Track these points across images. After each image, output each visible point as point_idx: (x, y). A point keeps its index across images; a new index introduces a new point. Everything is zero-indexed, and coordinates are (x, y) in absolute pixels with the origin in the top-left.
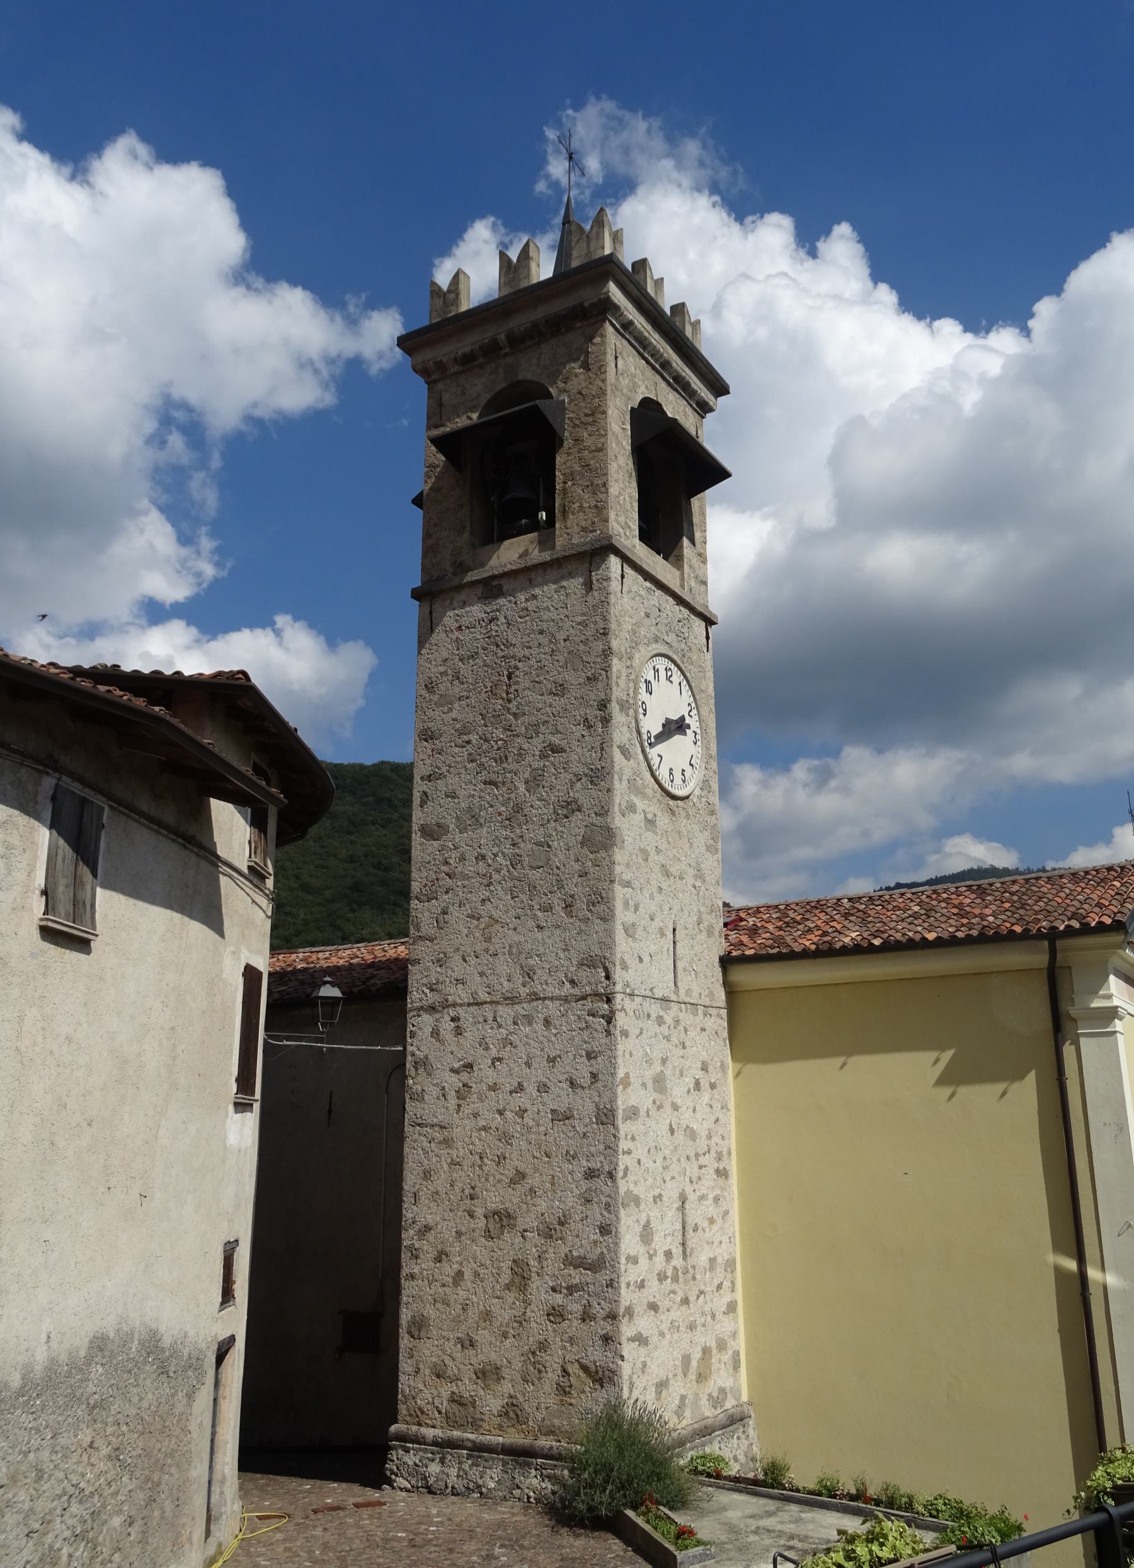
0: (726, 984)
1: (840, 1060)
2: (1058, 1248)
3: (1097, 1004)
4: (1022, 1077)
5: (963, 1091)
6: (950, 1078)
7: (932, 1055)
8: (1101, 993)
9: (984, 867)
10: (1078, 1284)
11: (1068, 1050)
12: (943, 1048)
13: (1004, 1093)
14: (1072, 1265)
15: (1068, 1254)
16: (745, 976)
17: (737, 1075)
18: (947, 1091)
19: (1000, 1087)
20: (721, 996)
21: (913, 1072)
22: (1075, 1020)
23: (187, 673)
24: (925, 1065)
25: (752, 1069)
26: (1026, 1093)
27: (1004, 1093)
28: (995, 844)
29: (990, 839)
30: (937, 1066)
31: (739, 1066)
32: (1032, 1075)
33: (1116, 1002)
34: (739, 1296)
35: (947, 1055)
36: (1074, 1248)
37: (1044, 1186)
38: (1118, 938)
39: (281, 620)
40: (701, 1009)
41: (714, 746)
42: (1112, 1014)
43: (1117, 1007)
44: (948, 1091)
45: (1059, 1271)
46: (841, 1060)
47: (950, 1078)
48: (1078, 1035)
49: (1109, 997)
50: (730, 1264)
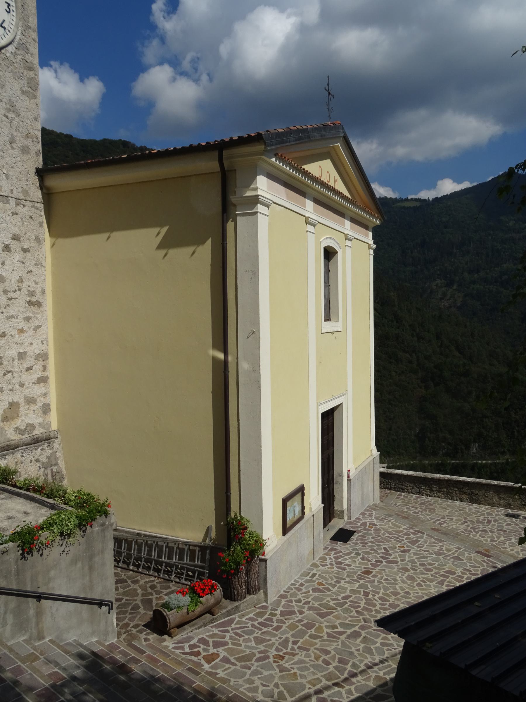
0: (42, 187)
1: (106, 235)
2: (215, 346)
3: (249, 193)
4: (203, 242)
5: (172, 252)
6: (166, 244)
7: (156, 230)
8: (251, 187)
9: (382, 197)
10: (223, 367)
11: (230, 225)
12: (162, 226)
13: (194, 253)
14: (221, 356)
15: (219, 350)
16: (60, 182)
17: (53, 245)
18: (163, 252)
19: (191, 249)
20: (38, 195)
21: (144, 240)
22: (235, 206)
23: (178, 148)
24: (150, 237)
25: (61, 241)
26: (205, 251)
27: (194, 253)
28: (388, 188)
29: (386, 186)
30: (158, 237)
31: (53, 240)
32: (209, 242)
33: (259, 192)
34: (51, 373)
35: (165, 229)
36: (222, 347)
37: (210, 309)
38: (261, 147)
39: (52, 63)
40: (12, 202)
41: (33, 22)
42: (255, 200)
43: (259, 195)
44: (163, 252)
45: (215, 360)
46: (107, 234)
47: (166, 244)
48: (236, 215)
49: (256, 189)
50: (43, 356)
